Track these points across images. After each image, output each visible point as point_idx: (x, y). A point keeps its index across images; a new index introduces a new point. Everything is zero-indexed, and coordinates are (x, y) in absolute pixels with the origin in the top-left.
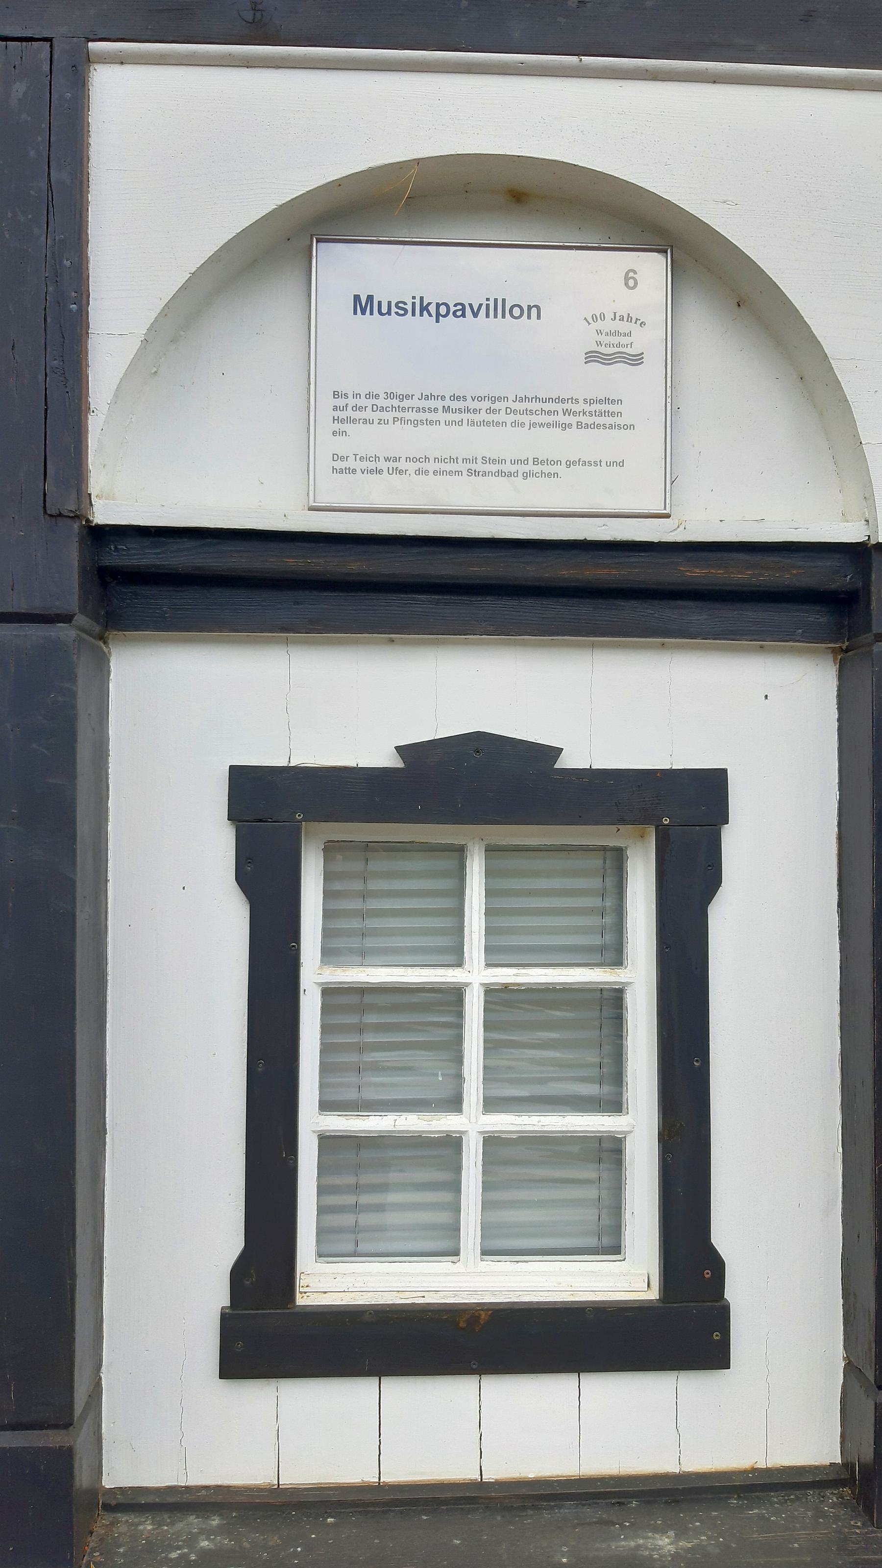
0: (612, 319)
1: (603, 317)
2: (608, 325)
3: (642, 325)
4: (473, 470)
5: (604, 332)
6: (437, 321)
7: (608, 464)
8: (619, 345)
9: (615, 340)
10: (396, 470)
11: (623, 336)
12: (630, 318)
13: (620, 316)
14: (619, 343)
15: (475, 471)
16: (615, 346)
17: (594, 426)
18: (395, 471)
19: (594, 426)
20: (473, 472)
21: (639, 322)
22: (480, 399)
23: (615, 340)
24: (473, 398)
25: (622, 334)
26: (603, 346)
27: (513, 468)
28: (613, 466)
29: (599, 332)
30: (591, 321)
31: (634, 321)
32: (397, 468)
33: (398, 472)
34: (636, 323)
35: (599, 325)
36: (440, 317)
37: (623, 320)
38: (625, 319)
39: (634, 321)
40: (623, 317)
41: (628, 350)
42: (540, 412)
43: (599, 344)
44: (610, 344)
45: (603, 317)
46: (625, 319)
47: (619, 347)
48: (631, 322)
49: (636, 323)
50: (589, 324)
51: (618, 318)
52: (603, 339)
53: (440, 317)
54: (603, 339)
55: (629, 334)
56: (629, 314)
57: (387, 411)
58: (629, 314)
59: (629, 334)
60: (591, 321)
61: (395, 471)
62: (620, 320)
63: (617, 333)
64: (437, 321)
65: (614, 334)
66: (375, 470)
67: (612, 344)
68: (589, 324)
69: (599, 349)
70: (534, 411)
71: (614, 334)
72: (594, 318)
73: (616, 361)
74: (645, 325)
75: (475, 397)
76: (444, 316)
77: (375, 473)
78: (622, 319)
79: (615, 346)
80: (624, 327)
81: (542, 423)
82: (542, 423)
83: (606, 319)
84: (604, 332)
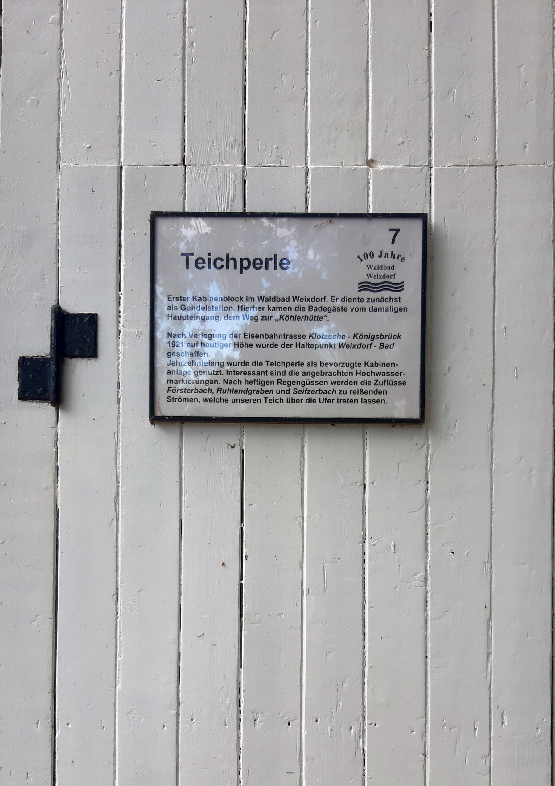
0: (379, 256)
1: (372, 255)
2: (376, 261)
3: (403, 260)
4: (172, 397)
5: (373, 267)
6: (241, 272)
7: (278, 392)
8: (385, 276)
9: (382, 272)
10: (326, 400)
11: (388, 269)
12: (393, 255)
13: (385, 254)
14: (385, 274)
15: (173, 398)
16: (382, 277)
17: (244, 364)
18: (324, 401)
19: (244, 364)
20: (172, 399)
21: (400, 258)
22: (357, 309)
23: (382, 272)
24: (352, 309)
25: (387, 268)
26: (373, 277)
27: (277, 396)
28: (282, 393)
29: (369, 267)
30: (362, 258)
31: (396, 257)
32: (326, 398)
33: (327, 401)
34: (398, 258)
35: (369, 261)
36: (243, 269)
37: (388, 257)
38: (390, 255)
39: (396, 257)
40: (388, 254)
41: (392, 280)
42: (337, 337)
43: (369, 276)
44: (378, 276)
45: (241, 299)
46: (390, 255)
47: (385, 278)
48: (394, 257)
49: (398, 258)
50: (361, 261)
51: (384, 255)
52: (374, 272)
53: (243, 269)
54: (374, 272)
55: (393, 268)
56: (392, 252)
57: (386, 302)
58: (392, 252)
59: (393, 268)
60: (362, 258)
61: (324, 401)
62: (385, 257)
63: (383, 267)
64: (241, 272)
65: (381, 268)
66: (213, 399)
67: (380, 276)
68: (361, 261)
69: (370, 280)
70: (332, 336)
71: (381, 268)
72: (366, 256)
73: (389, 289)
74: (405, 260)
75: (353, 308)
76: (246, 268)
77: (213, 401)
78: (387, 255)
79: (382, 277)
80: (389, 262)
81: (230, 362)
82: (230, 362)
83: (374, 257)
84: (373, 267)
